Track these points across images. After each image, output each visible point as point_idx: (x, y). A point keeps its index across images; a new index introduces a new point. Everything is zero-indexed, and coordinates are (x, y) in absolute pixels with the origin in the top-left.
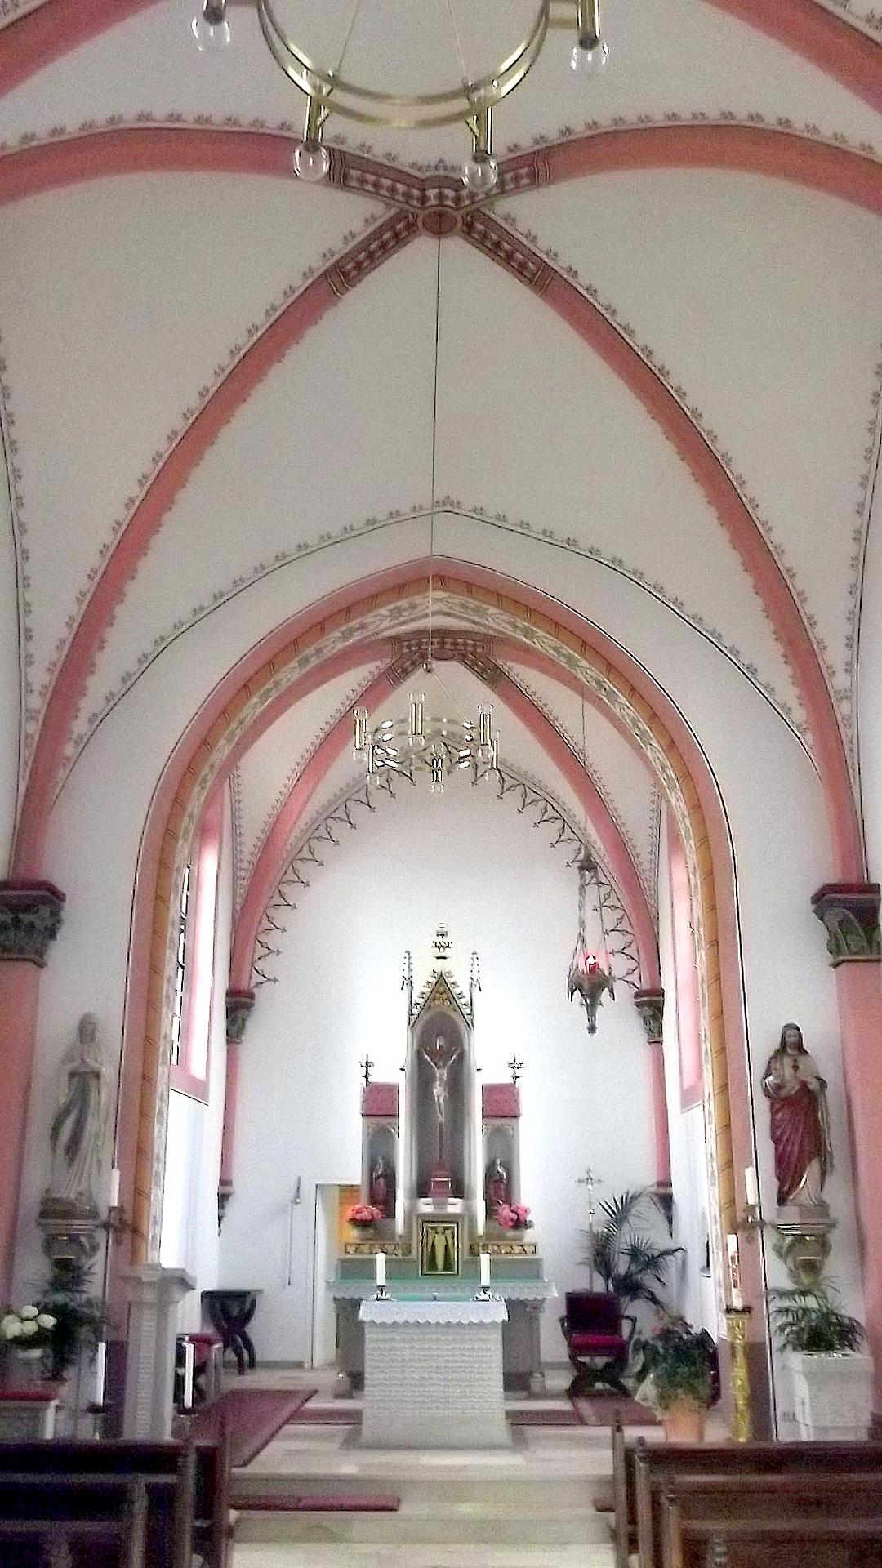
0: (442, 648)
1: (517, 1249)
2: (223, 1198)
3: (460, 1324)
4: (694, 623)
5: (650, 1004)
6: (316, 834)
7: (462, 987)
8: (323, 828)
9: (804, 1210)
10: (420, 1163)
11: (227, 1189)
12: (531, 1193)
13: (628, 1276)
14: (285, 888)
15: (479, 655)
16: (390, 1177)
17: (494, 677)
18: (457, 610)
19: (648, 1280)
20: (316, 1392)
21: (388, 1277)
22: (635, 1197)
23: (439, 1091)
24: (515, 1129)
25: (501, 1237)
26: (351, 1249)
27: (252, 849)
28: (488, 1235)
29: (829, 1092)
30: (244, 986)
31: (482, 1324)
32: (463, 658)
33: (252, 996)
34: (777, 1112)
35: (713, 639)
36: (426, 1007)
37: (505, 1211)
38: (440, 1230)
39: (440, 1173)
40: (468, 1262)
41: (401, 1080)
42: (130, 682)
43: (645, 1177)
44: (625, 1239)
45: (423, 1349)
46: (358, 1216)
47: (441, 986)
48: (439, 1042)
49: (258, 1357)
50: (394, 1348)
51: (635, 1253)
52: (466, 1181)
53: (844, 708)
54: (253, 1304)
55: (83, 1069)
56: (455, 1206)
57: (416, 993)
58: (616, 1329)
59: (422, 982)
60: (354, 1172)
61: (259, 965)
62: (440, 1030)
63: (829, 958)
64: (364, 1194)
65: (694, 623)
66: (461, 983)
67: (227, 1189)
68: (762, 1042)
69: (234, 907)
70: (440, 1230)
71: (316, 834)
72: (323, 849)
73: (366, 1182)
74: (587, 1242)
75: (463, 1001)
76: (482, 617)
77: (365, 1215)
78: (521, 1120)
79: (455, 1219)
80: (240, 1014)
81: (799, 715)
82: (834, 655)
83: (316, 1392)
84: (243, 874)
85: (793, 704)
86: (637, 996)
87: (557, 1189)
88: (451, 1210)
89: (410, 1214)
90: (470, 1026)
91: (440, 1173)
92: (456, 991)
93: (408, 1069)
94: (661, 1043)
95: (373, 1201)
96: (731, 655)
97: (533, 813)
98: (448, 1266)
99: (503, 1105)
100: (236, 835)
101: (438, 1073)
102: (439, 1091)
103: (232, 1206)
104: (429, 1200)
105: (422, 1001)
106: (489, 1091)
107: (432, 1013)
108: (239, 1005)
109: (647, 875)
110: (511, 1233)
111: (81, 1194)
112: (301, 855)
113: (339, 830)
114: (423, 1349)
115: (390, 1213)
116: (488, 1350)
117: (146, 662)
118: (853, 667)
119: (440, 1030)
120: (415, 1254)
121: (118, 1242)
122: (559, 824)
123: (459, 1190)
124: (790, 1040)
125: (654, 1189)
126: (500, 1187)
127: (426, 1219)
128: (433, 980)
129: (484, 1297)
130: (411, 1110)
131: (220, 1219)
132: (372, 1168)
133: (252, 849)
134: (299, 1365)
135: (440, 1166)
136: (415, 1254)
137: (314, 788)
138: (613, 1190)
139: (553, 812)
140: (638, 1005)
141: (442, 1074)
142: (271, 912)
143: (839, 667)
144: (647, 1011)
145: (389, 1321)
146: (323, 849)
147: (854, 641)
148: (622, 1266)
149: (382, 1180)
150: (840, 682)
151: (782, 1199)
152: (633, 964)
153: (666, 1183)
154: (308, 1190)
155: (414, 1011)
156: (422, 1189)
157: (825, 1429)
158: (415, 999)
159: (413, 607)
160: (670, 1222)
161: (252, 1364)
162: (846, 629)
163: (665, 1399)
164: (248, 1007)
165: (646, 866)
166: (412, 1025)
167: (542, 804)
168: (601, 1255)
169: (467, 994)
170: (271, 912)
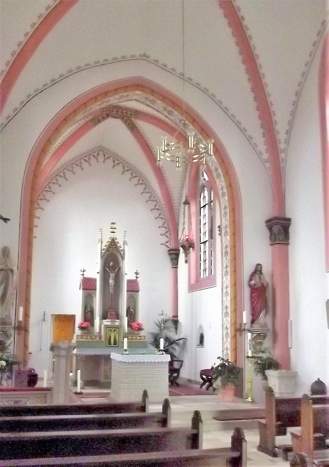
1: (138, 338)
3: (155, 362)
4: (232, 117)
6: (52, 181)
7: (121, 244)
9: (261, 326)
10: (103, 307)
12: (141, 318)
15: (128, 117)
16: (92, 312)
17: (133, 128)
18: (143, 100)
21: (128, 347)
22: (168, 320)
23: (111, 281)
24: (138, 296)
26: (79, 337)
29: (269, 286)
31: (162, 362)
32: (122, 118)
34: (253, 293)
35: (238, 124)
36: (107, 250)
38: (113, 331)
39: (110, 312)
41: (98, 277)
42: (17, 112)
43: (169, 314)
47: (113, 243)
53: (282, 155)
55: (6, 268)
59: (106, 240)
62: (112, 258)
63: (269, 242)
65: (232, 117)
66: (120, 242)
68: (247, 269)
70: (113, 331)
71: (52, 181)
76: (153, 104)
78: (140, 293)
81: (265, 156)
82: (281, 136)
85: (263, 151)
86: (169, 251)
90: (123, 258)
91: (110, 312)
92: (119, 245)
94: (177, 268)
96: (243, 130)
97: (135, 181)
98: (115, 343)
99: (133, 287)
101: (111, 275)
102: (111, 281)
106: (129, 282)
107: (108, 253)
109: (176, 208)
111: (6, 316)
112: (147, 188)
113: (61, 180)
115: (92, 325)
117: (24, 104)
118: (287, 142)
119: (112, 258)
120: (103, 339)
121: (241, 325)
123: (117, 316)
124: (259, 269)
125: (171, 319)
126: (132, 314)
127: (107, 327)
136: (103, 339)
138: (165, 318)
139: (142, 181)
140: (170, 254)
141: (112, 275)
143: (282, 141)
145: (131, 361)
146: (54, 187)
147: (288, 132)
149: (89, 313)
150: (282, 146)
151: (253, 322)
152: (168, 239)
156: (104, 317)
157: (282, 393)
158: (103, 247)
159: (127, 96)
160: (176, 329)
162: (287, 127)
163: (224, 385)
165: (176, 204)
169: (122, 246)
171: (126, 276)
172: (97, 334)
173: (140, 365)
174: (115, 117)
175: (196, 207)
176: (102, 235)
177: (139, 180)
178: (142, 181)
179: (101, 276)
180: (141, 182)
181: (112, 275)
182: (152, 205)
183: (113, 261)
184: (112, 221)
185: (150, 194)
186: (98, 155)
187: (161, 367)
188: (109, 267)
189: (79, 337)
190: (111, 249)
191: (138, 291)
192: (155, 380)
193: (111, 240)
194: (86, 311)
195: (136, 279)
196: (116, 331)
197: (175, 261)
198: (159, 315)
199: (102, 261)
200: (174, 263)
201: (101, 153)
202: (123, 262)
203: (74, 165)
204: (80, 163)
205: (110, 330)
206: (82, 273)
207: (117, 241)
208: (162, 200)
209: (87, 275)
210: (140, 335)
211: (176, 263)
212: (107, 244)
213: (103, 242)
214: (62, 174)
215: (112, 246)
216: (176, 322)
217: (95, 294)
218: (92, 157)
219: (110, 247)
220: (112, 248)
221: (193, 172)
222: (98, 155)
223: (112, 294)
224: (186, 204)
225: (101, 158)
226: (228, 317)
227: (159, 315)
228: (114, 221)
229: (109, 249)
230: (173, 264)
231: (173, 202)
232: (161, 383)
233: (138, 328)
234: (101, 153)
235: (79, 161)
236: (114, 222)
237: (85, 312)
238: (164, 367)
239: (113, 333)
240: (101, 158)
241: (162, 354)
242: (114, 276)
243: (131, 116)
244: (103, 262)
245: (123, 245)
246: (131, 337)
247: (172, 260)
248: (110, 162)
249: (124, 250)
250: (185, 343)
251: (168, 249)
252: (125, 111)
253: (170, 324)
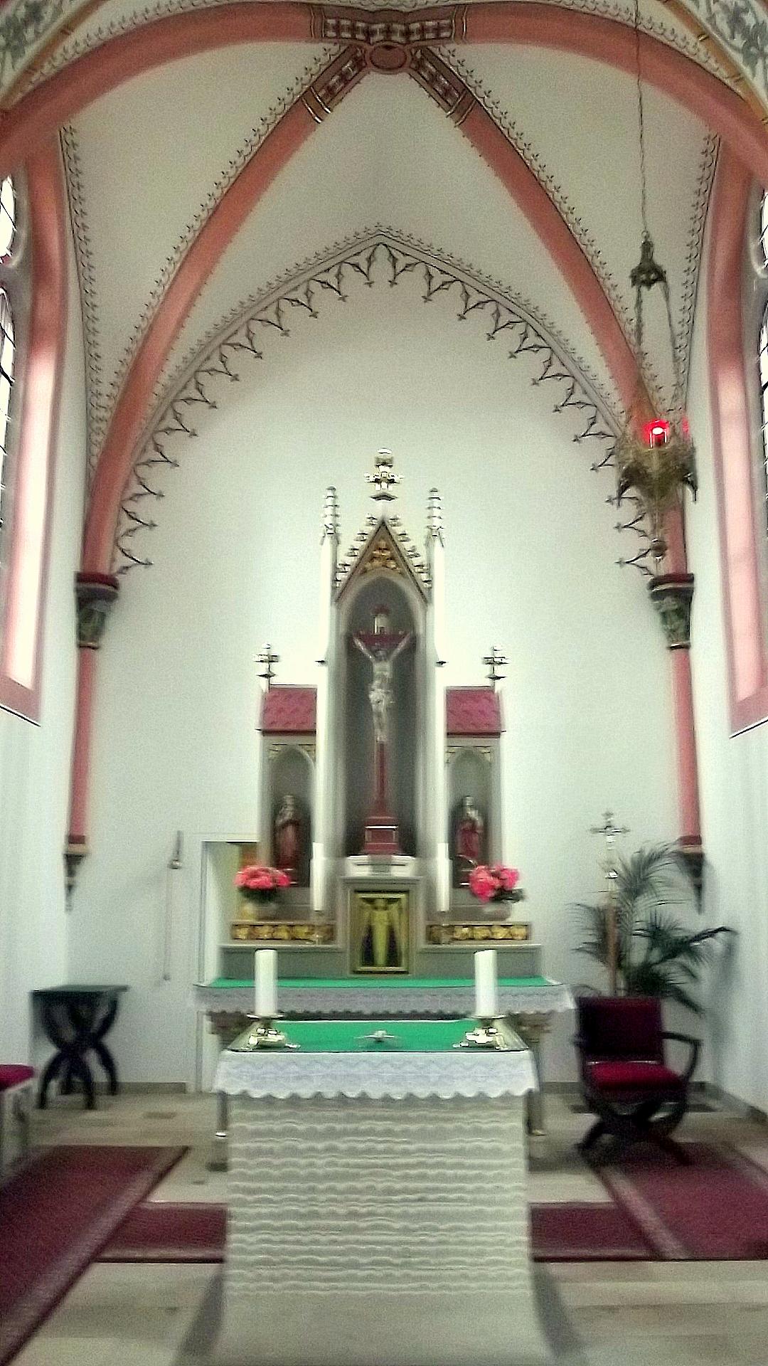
0: (388, 38)
1: (501, 933)
2: (72, 861)
3: (434, 1100)
5: (676, 593)
8: (216, 357)
11: (77, 849)
12: (518, 846)
13: (647, 966)
14: (162, 438)
16: (303, 825)
19: (674, 972)
20: (185, 1150)
22: (653, 859)
24: (495, 752)
25: (474, 914)
26: (243, 933)
27: (113, 378)
28: (455, 912)
30: (104, 568)
31: (481, 1100)
33: (115, 585)
36: (359, 570)
37: (481, 874)
38: (381, 903)
40: (424, 953)
43: (663, 830)
44: (643, 910)
45: (353, 1152)
46: (253, 883)
47: (382, 539)
48: (379, 623)
49: (124, 1077)
50: (294, 1152)
51: (656, 934)
52: (420, 825)
54: (114, 1007)
56: (403, 868)
57: (344, 549)
58: (657, 1052)
60: (249, 824)
61: (126, 543)
62: (381, 606)
64: (264, 855)
67: (77, 849)
69: (88, 460)
70: (381, 903)
72: (215, 386)
73: (267, 835)
74: (589, 922)
75: (416, 561)
77: (264, 881)
79: (405, 887)
80: (98, 606)
83: (185, 1150)
84: (102, 413)
86: (653, 585)
87: (553, 846)
88: (397, 872)
89: (336, 881)
90: (426, 599)
91: (381, 818)
93: (332, 659)
94: (687, 647)
95: (278, 860)
97: (509, 338)
98: (393, 956)
99: (476, 717)
100: (91, 358)
102: (378, 696)
103: (86, 872)
104: (363, 858)
105: (351, 560)
106: (457, 698)
107: (365, 581)
108: (95, 595)
110: (490, 909)
114: (353, 1152)
115: (303, 879)
116: (496, 1153)
119: (381, 606)
120: (341, 941)
122: (545, 354)
123: (410, 843)
126: (473, 836)
127: (358, 887)
128: (370, 530)
129: (482, 1038)
130: (335, 727)
131: (70, 888)
132: (275, 808)
133: (113, 378)
134: (179, 1089)
135: (381, 806)
136: (341, 941)
137: (197, 292)
138: (628, 849)
139: (533, 333)
140: (656, 596)
141: (383, 669)
142: (143, 471)
144: (670, 603)
146: (215, 386)
148: (639, 952)
149: (290, 831)
153: (696, 839)
154: (193, 853)
155: (340, 576)
156: (352, 843)
158: (343, 558)
160: (699, 888)
161: (114, 1087)
164: (111, 597)
166: (338, 596)
167: (520, 328)
168: (606, 935)
169: (421, 550)
170: (143, 471)
171: (439, 671)
172: (315, 920)
173: (341, 1114)
174: (390, 69)
175: (744, 385)
176: (338, 511)
177: (549, 363)
178: (533, 333)
179: (335, 678)
180: (532, 340)
181: (383, 669)
182: (577, 419)
183: (382, 610)
184: (376, 453)
185: (568, 382)
186: (370, 260)
187: (478, 1132)
188: (369, 639)
189: (243, 933)
190: (376, 563)
191: (497, 734)
192: (443, 1208)
193: (372, 528)
194: (280, 821)
195: (488, 682)
196: (394, 906)
197: (678, 623)
198: (596, 831)
199: (338, 613)
200: (673, 631)
201: (382, 253)
202: (429, 614)
203: (285, 305)
204: (308, 293)
205: (371, 901)
206: (263, 668)
207: (399, 530)
208: (615, 397)
209: (286, 676)
210: (510, 920)
211: (681, 631)
212: (359, 545)
213: (342, 539)
214: (241, 339)
215: (377, 552)
216: (694, 864)
217: (312, 747)
218: (348, 270)
219: (373, 558)
220: (379, 558)
221: (723, 254)
222: (370, 260)
223: (382, 745)
224: (649, 284)
225: (382, 269)
226: (14, 58)
227: (596, 831)
228: (389, 453)
229: (368, 565)
230: (672, 633)
231: (657, 395)
232: (480, 1229)
233: (493, 888)
234: (382, 253)
235: (302, 289)
236: (388, 457)
237: (274, 822)
238: (498, 1132)
239: (385, 913)
240: (382, 269)
241: (489, 1047)
242: (387, 674)
243: (438, 35)
244: (343, 618)
245: (427, 545)
246: (466, 930)
247: (664, 615)
248: (414, 282)
249: (430, 565)
250: (730, 951)
251: (650, 578)
252: (417, 25)
253: (669, 873)
